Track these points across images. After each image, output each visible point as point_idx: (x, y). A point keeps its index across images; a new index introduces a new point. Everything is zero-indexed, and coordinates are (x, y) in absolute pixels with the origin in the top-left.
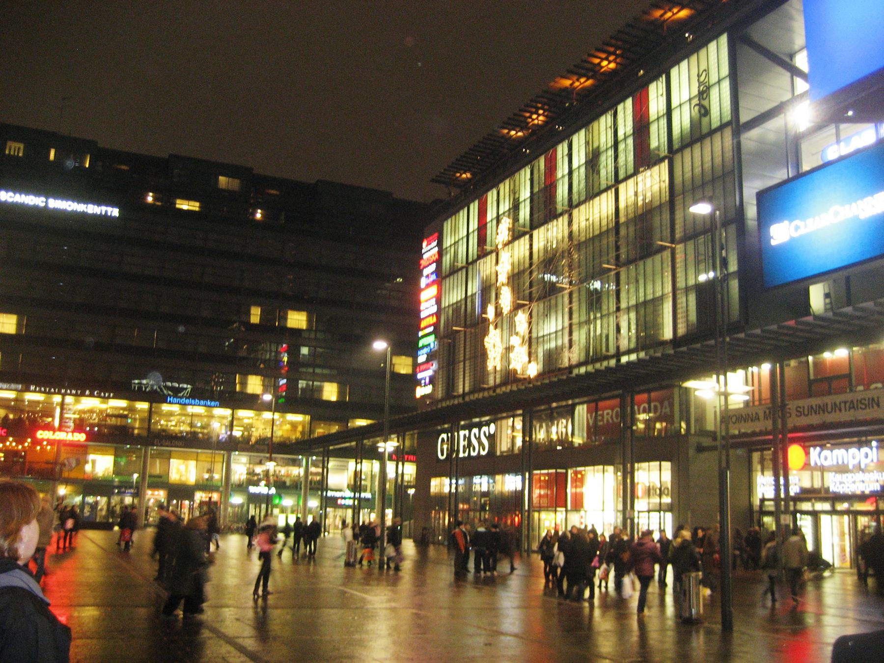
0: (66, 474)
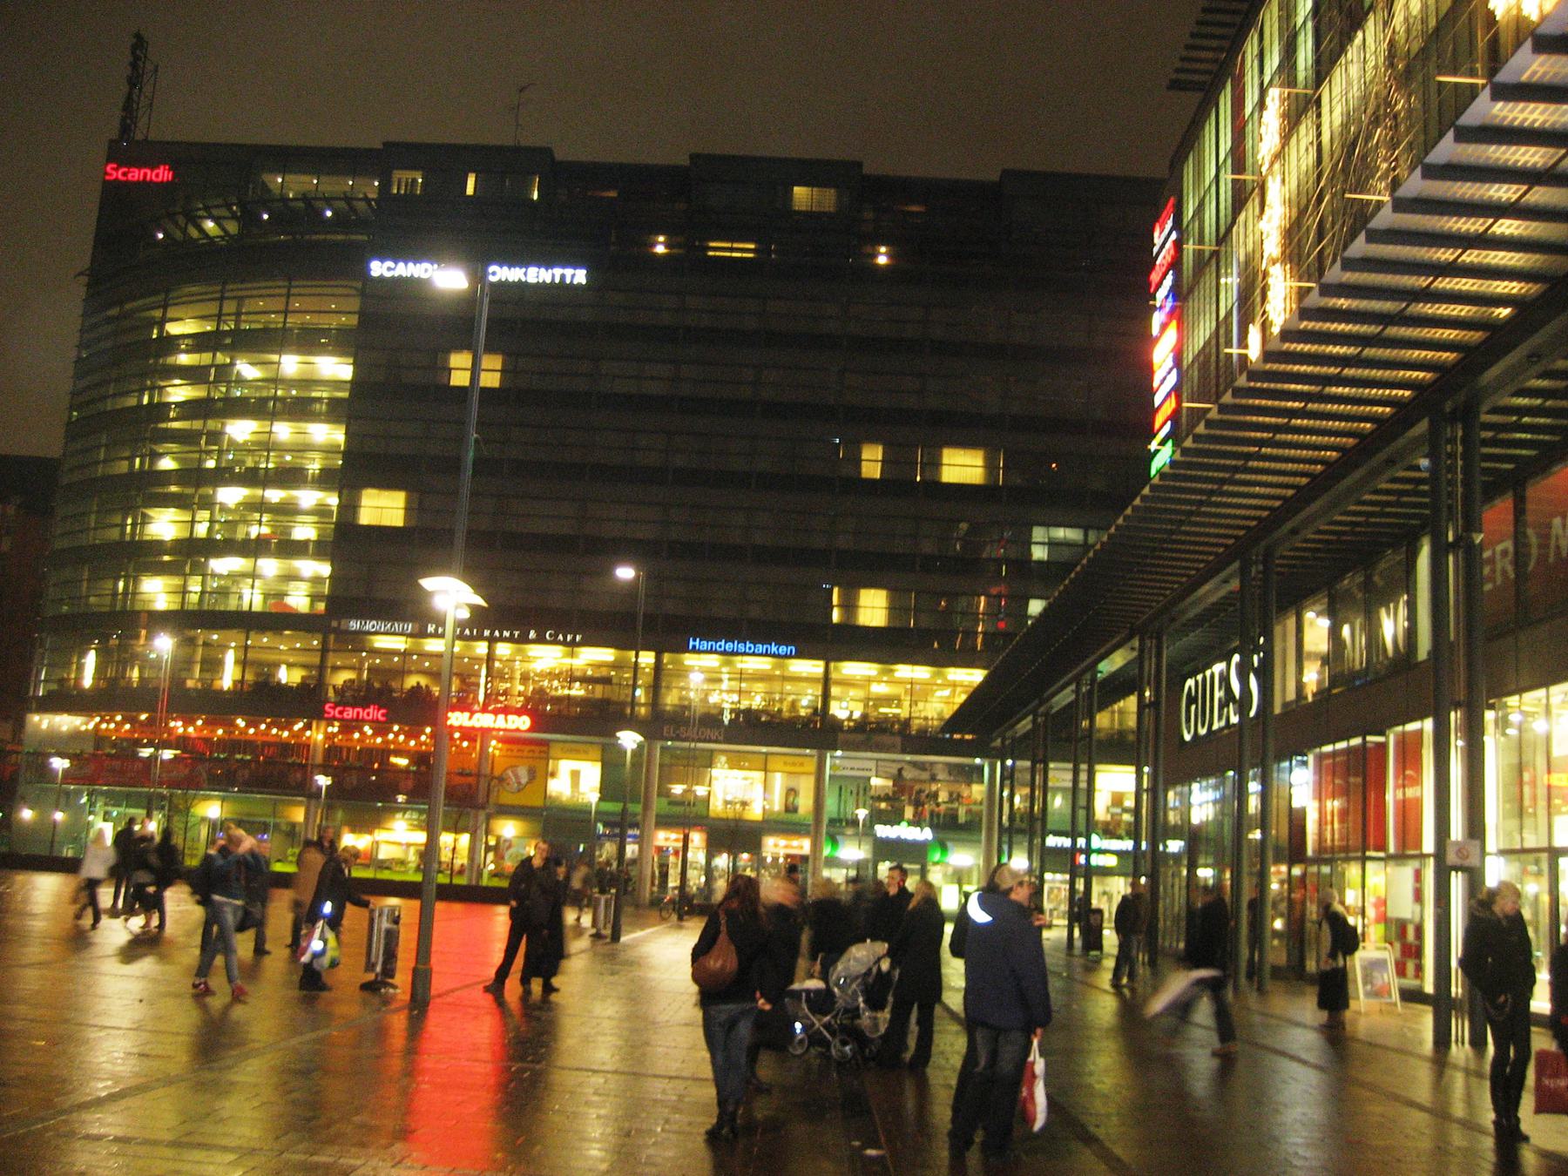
0: (507, 798)
